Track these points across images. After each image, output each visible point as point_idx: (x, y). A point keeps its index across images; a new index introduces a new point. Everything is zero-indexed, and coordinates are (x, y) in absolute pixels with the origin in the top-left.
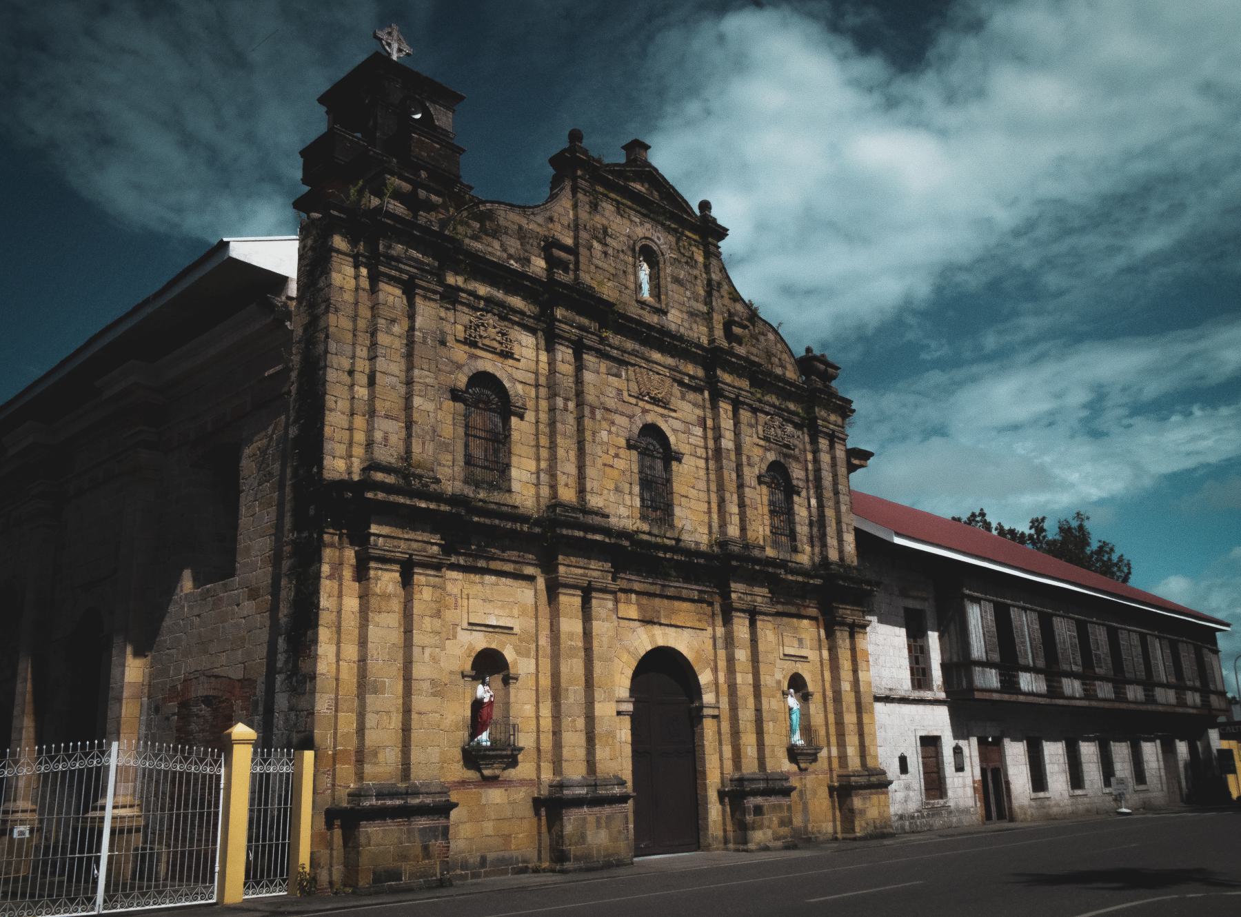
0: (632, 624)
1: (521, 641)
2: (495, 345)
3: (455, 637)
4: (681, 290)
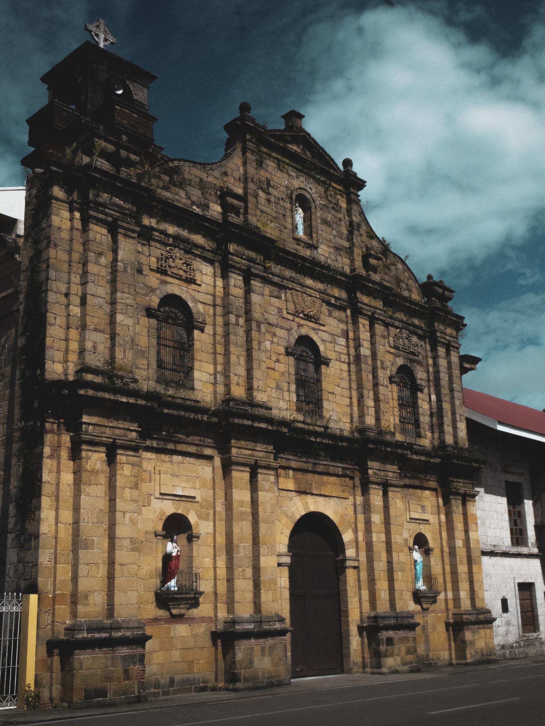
1: (202, 507)
2: (181, 273)
3: (149, 504)
4: (329, 229)
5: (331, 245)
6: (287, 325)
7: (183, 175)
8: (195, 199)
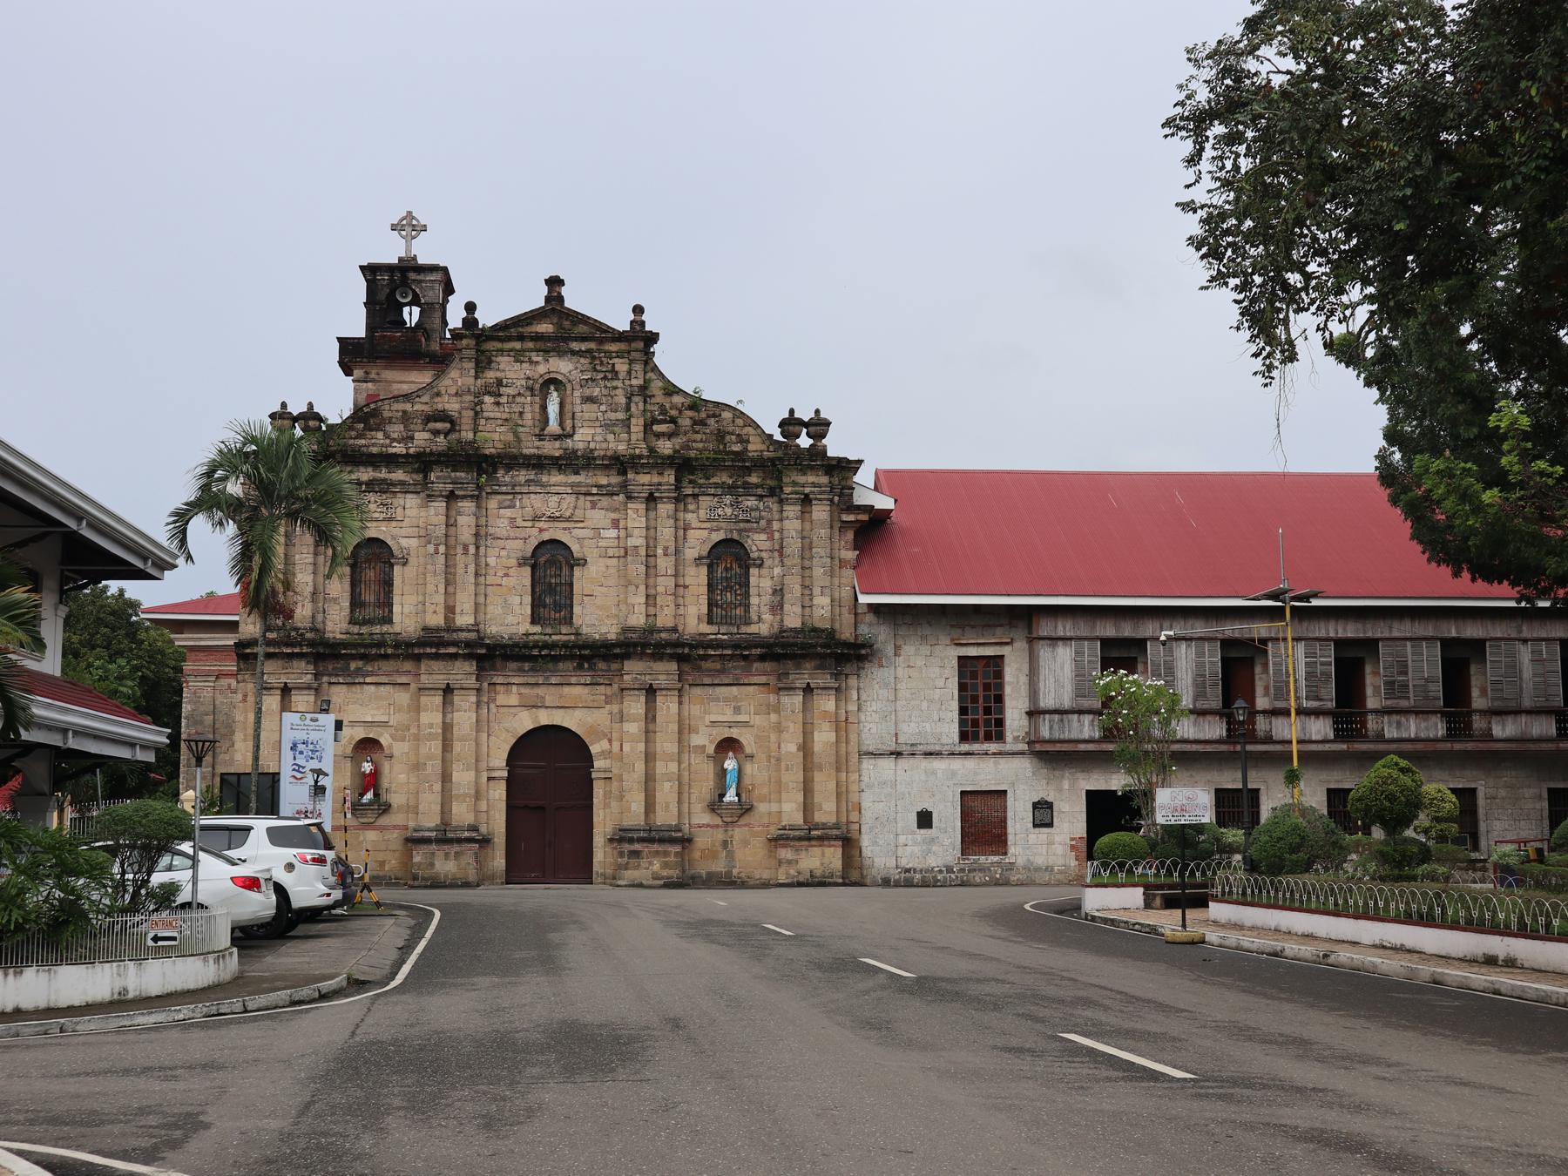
0: (513, 710)
1: (396, 730)
4: (595, 407)
5: (598, 424)
8: (395, 436)
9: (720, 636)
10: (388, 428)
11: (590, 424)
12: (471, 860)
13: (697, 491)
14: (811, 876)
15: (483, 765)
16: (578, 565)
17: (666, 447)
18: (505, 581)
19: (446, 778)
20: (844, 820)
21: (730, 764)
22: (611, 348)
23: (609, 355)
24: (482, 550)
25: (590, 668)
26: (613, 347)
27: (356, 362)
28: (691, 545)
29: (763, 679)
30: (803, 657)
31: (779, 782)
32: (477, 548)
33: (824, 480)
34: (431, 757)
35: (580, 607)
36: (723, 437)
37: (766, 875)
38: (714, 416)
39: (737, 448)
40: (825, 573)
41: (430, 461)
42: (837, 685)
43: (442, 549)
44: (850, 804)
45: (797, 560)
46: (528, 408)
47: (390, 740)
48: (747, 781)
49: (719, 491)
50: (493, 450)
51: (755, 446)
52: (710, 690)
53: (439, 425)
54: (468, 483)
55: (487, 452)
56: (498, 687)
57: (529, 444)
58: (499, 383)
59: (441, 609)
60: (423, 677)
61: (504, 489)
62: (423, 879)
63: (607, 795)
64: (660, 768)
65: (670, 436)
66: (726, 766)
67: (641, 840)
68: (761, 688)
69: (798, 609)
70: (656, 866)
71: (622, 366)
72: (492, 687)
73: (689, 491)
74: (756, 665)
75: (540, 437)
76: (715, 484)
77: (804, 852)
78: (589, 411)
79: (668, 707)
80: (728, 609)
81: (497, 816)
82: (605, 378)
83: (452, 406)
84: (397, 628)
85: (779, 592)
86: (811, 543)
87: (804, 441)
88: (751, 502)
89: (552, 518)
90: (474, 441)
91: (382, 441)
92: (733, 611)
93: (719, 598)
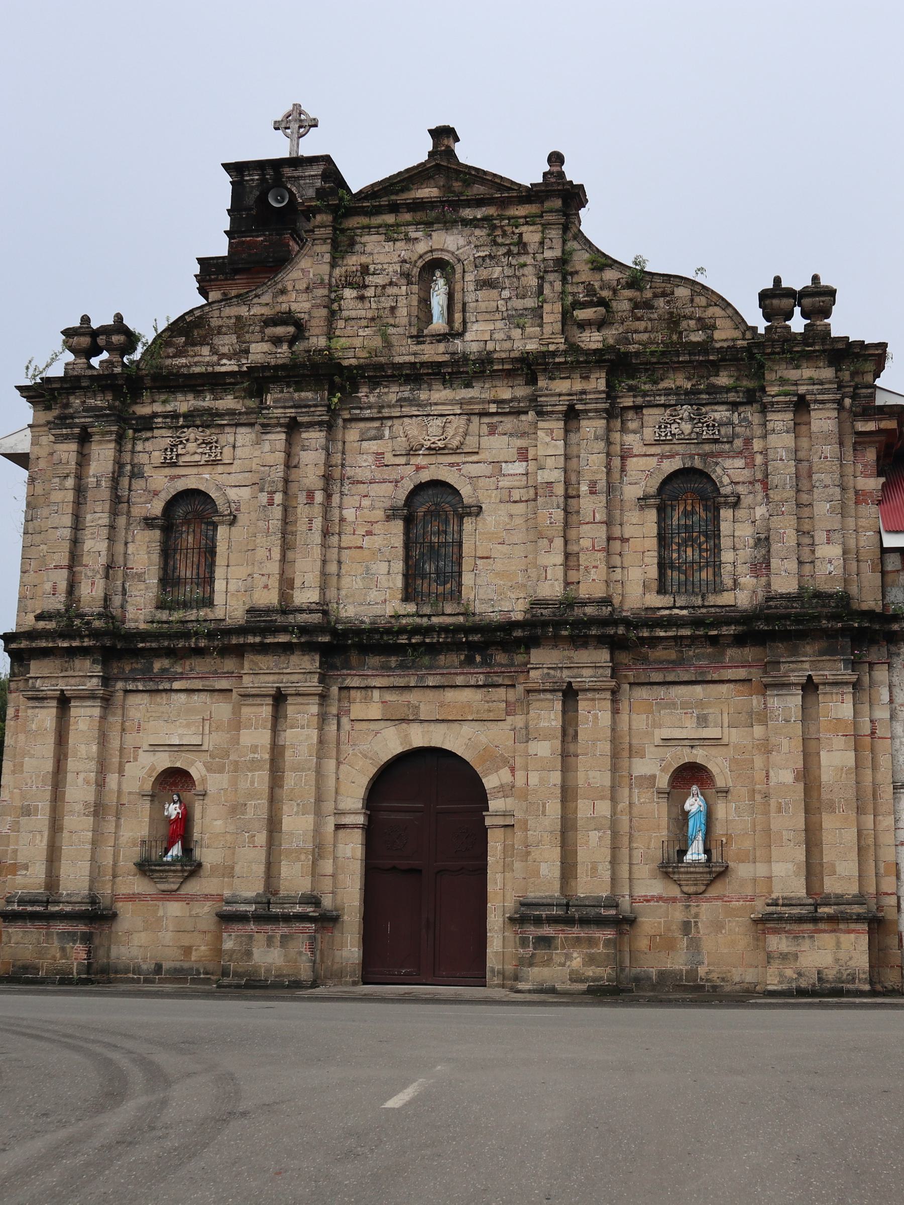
0: (372, 726)
2: (197, 458)
3: (136, 759)
4: (494, 293)
5: (498, 316)
6: (394, 474)
7: (209, 325)
8: (225, 350)
9: (676, 611)
10: (217, 341)
11: (488, 317)
12: (305, 949)
13: (639, 401)
14: (820, 979)
15: (329, 807)
16: (469, 514)
17: (592, 340)
18: (367, 542)
19: (273, 825)
20: (872, 890)
21: (694, 804)
22: (517, 213)
23: (514, 221)
24: (336, 499)
25: (484, 663)
26: (520, 211)
27: (211, 280)
28: (633, 479)
29: (742, 673)
30: (802, 635)
31: (767, 831)
32: (329, 496)
33: (828, 373)
34: (252, 795)
35: (472, 575)
36: (677, 323)
37: (750, 976)
38: (664, 294)
39: (697, 337)
40: (832, 511)
41: (264, 377)
42: (854, 678)
43: (278, 498)
44: (882, 865)
45: (790, 493)
46: (402, 302)
47: (204, 771)
48: (719, 830)
49: (672, 400)
50: (353, 362)
51: (724, 334)
52: (661, 691)
53: (280, 330)
54: (315, 406)
55: (345, 363)
56: (353, 693)
57: (403, 350)
58: (365, 270)
59: (274, 583)
60: (247, 680)
61: (367, 413)
62: (236, 974)
63: (507, 850)
64: (583, 809)
65: (600, 324)
66: (687, 806)
67: (553, 920)
68: (739, 687)
69: (792, 565)
70: (577, 961)
71: (532, 236)
72: (344, 693)
73: (628, 402)
74: (730, 652)
75: (419, 338)
76: (666, 389)
77: (807, 941)
78: (486, 299)
79: (596, 717)
80: (689, 572)
81: (348, 882)
82: (509, 253)
83: (300, 305)
84: (219, 613)
85: (763, 542)
86: (811, 467)
87: (797, 324)
88: (720, 413)
89: (434, 451)
90: (329, 348)
91: (207, 359)
92: (697, 575)
93: (675, 555)
